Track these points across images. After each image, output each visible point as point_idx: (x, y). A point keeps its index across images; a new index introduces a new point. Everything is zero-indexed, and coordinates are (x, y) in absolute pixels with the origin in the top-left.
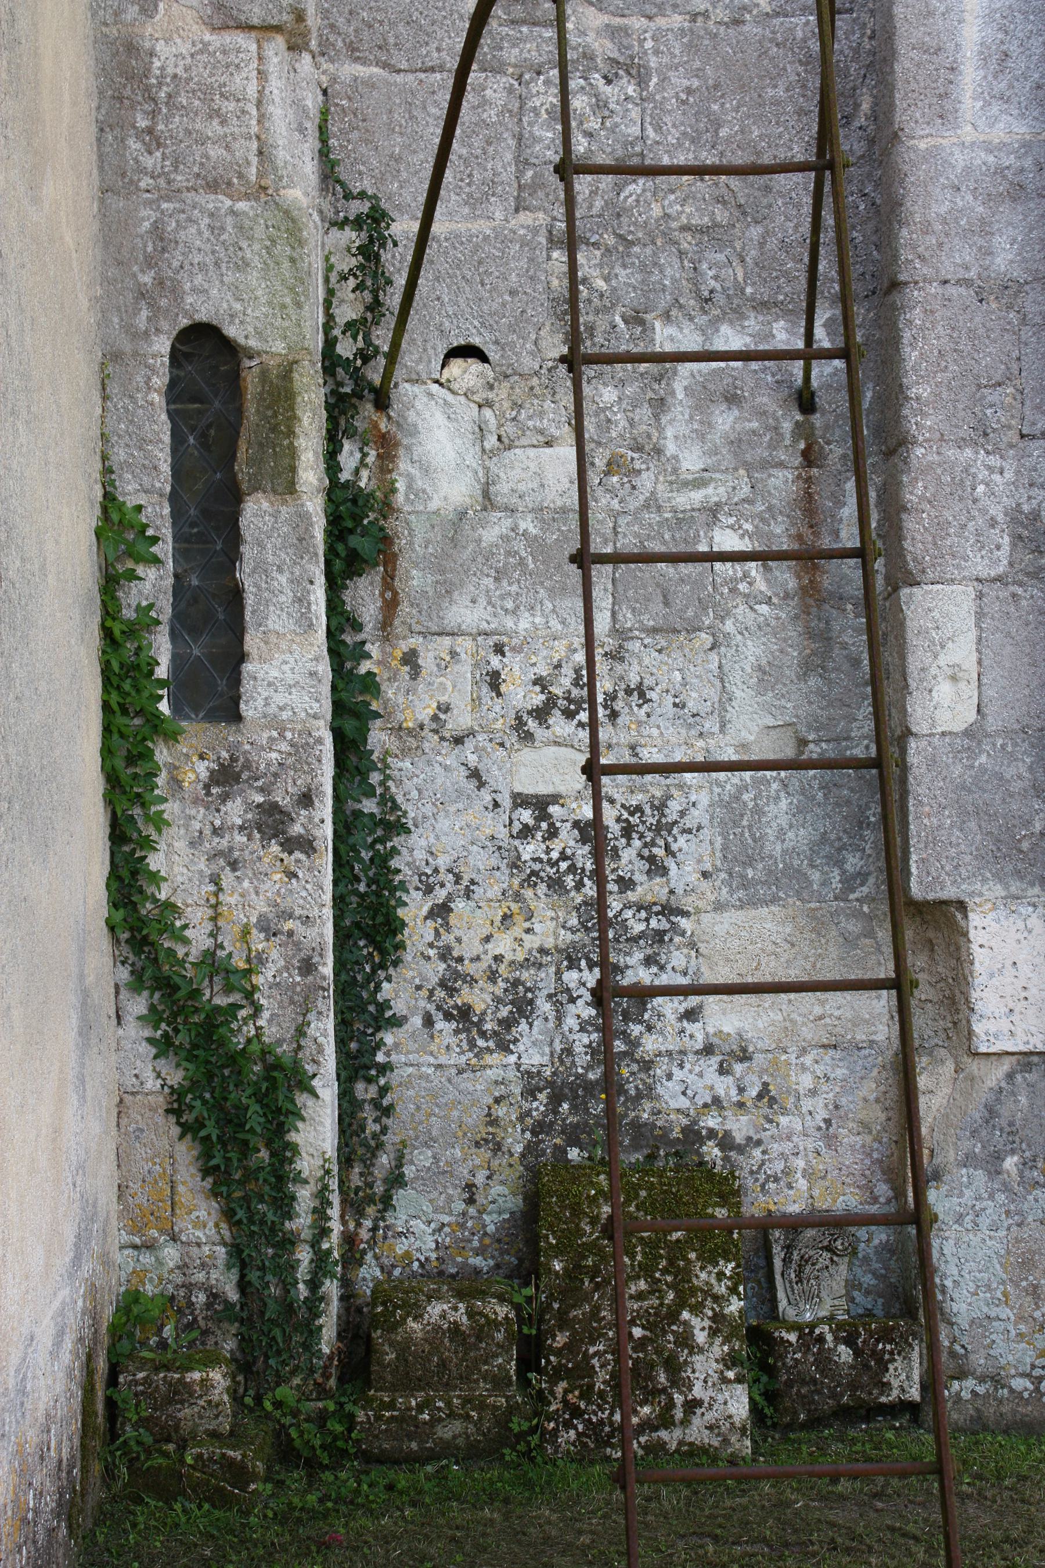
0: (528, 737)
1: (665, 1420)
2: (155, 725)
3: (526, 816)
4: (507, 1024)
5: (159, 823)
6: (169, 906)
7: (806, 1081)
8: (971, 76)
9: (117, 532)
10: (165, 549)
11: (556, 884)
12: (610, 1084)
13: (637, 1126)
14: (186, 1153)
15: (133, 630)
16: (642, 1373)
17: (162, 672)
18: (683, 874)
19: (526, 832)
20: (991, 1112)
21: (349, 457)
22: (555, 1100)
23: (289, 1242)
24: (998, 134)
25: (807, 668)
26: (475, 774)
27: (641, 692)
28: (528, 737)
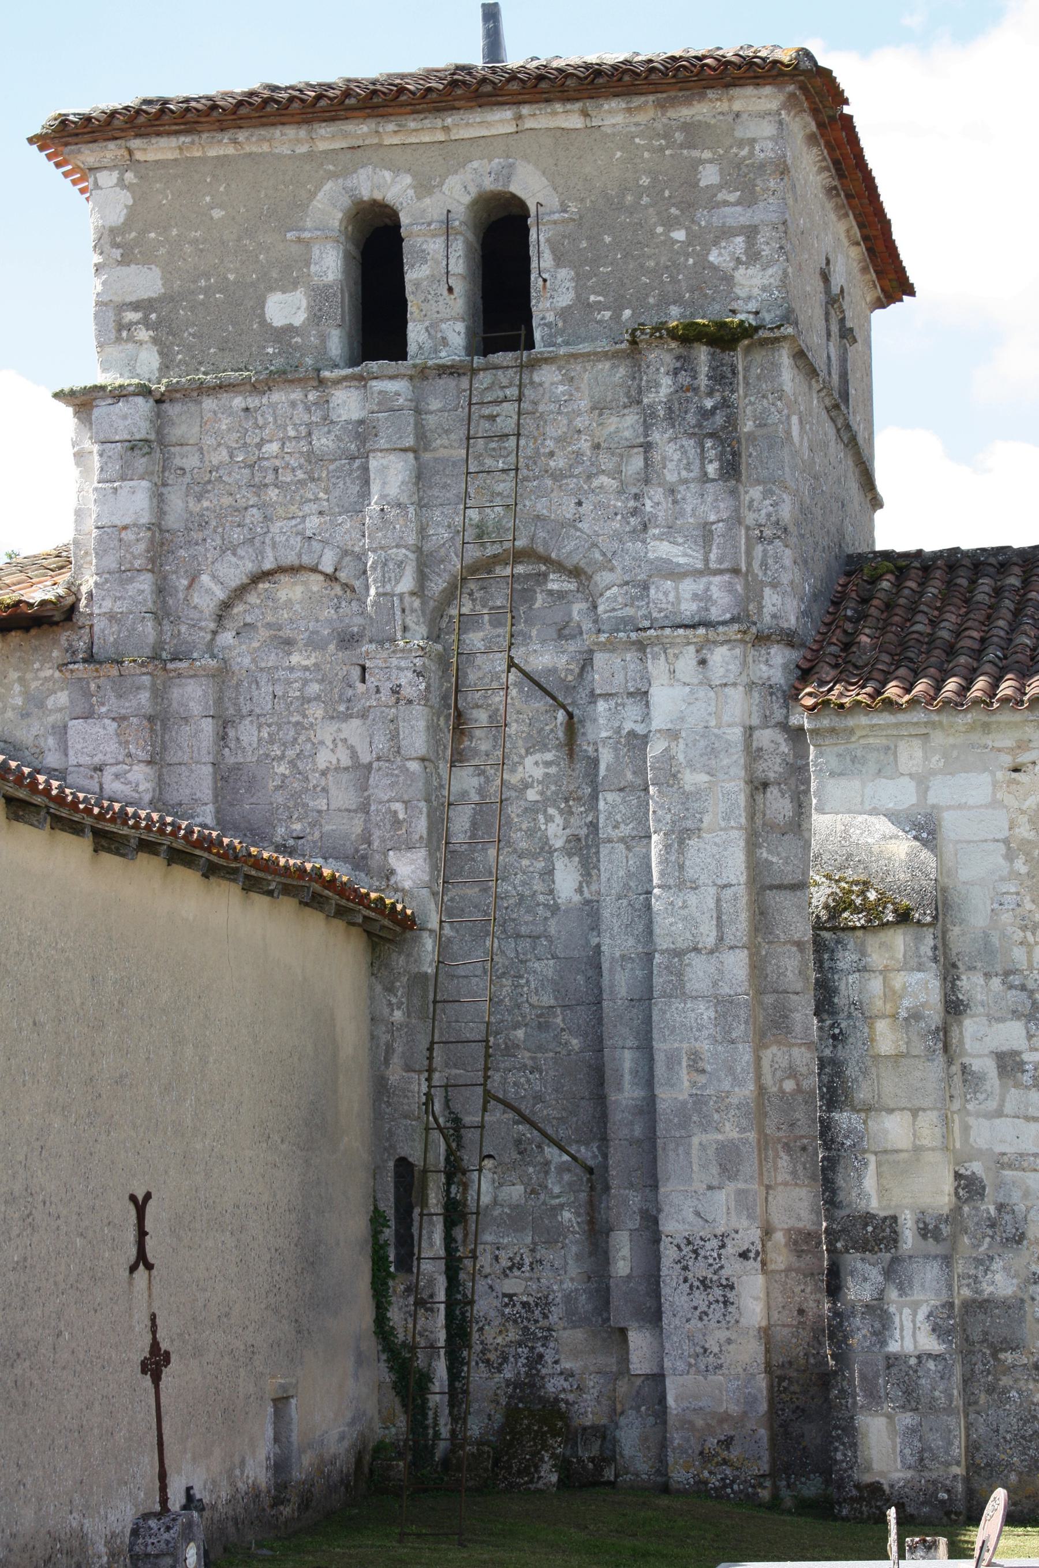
0: (506, 1276)
1: (531, 1481)
2: (389, 1275)
3: (506, 1300)
4: (501, 1364)
5: (390, 1303)
6: (393, 1328)
7: (592, 1384)
8: (627, 1077)
9: (377, 1220)
10: (392, 1223)
11: (515, 1321)
12: (532, 1385)
13: (540, 1397)
14: (397, 1400)
15: (382, 1247)
16: (527, 1467)
17: (392, 1258)
18: (554, 1318)
19: (506, 1305)
20: (638, 1393)
21: (454, 1189)
22: (515, 1388)
23: (426, 1427)
24: (636, 1094)
25: (591, 1254)
26: (491, 1287)
27: (541, 1262)
28: (506, 1276)
